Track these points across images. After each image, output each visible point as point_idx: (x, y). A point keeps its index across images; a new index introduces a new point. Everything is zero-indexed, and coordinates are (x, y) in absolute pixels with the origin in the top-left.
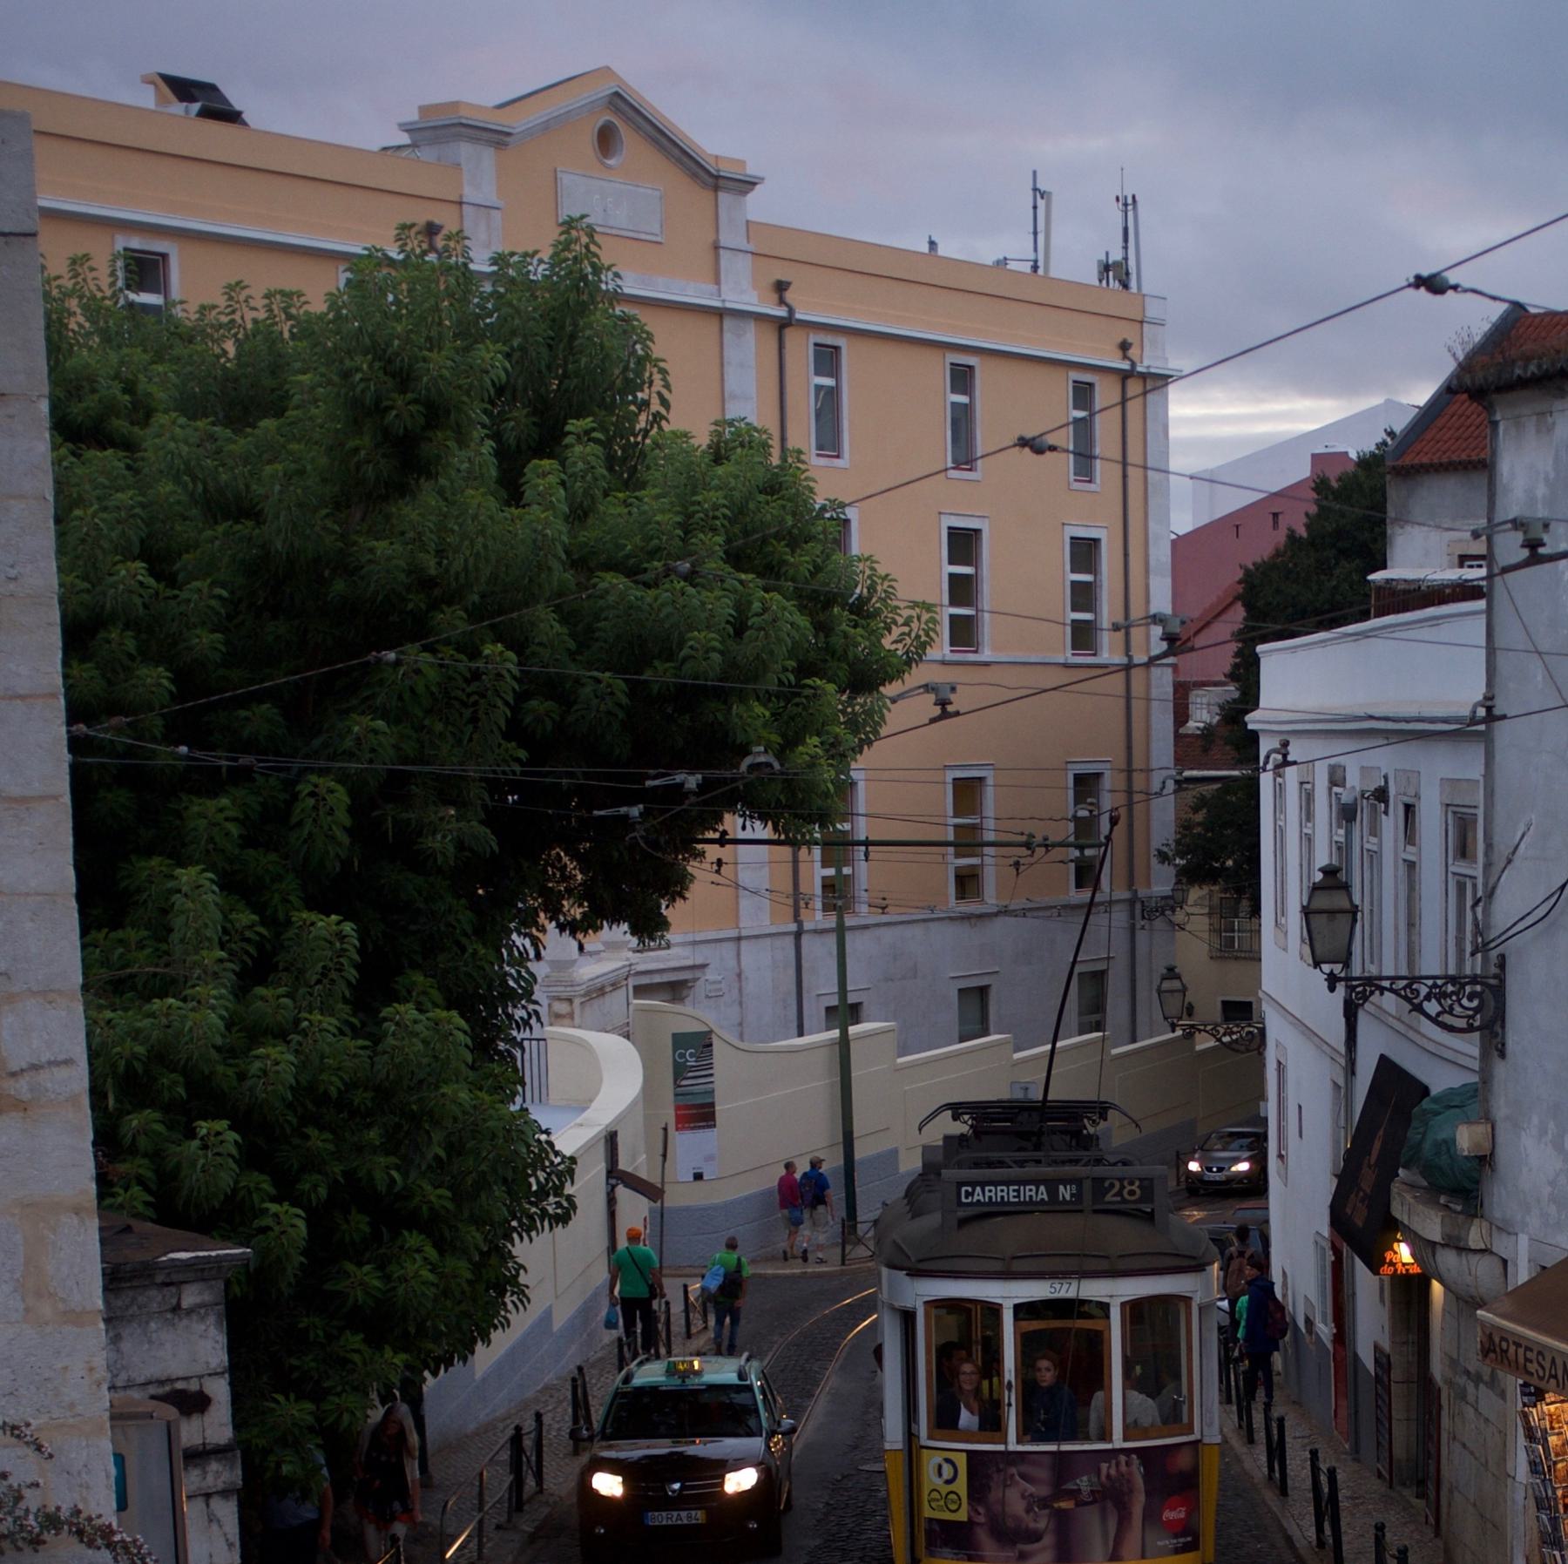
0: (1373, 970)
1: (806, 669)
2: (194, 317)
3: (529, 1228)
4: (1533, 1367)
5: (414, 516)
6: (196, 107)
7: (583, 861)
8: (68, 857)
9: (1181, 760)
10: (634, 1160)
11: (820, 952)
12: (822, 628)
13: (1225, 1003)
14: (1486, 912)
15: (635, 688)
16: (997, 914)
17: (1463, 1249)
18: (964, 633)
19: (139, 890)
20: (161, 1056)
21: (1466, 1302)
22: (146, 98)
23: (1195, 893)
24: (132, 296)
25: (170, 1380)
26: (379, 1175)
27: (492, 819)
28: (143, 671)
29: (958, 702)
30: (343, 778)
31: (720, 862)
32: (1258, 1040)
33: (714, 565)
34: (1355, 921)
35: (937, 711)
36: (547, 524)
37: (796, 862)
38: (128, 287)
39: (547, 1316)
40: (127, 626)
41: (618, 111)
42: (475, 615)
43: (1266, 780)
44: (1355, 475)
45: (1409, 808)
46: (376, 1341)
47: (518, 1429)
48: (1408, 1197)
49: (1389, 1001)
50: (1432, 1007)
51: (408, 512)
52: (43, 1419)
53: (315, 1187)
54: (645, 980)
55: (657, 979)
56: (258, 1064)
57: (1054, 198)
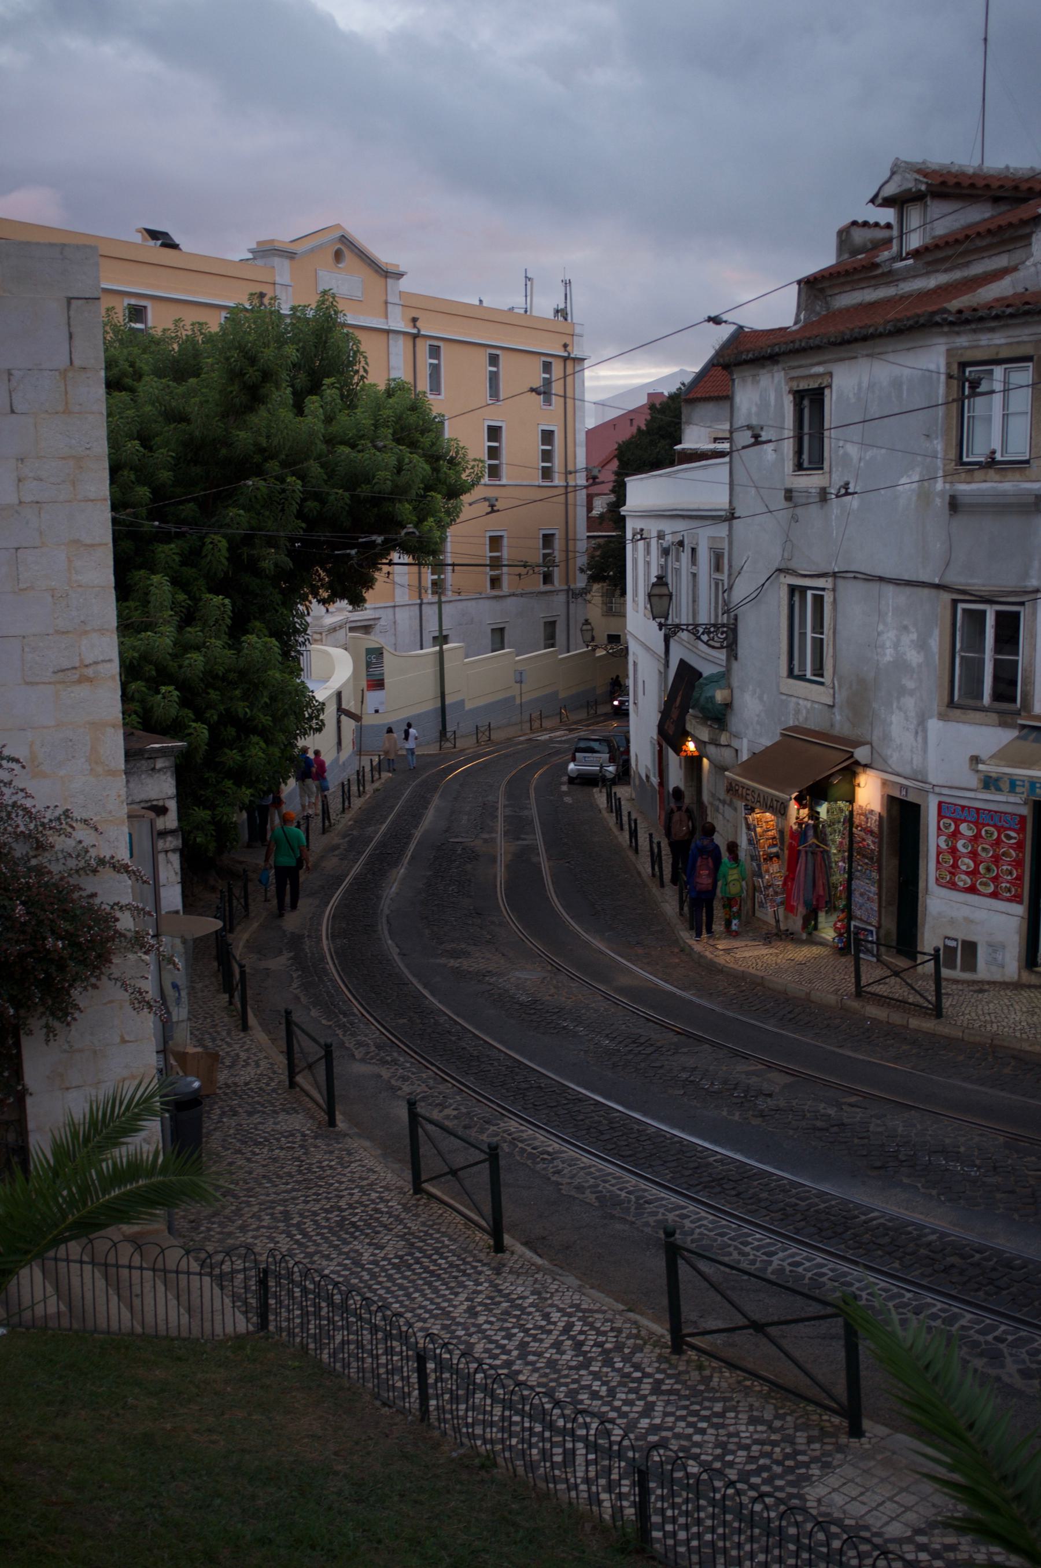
0: (677, 621)
1: (428, 488)
2: (160, 334)
4: (749, 798)
5: (256, 421)
6: (159, 242)
8: (111, 570)
10: (349, 704)
11: (430, 613)
12: (436, 470)
14: (729, 596)
17: (718, 745)
18: (494, 472)
19: (135, 584)
20: (145, 657)
21: (719, 768)
22: (138, 238)
23: (596, 587)
24: (133, 325)
25: (150, 801)
26: (240, 710)
27: (290, 553)
28: (138, 489)
29: (499, 506)
30: (225, 536)
31: (389, 573)
35: (489, 509)
37: (420, 573)
38: (130, 321)
40: (131, 469)
41: (343, 243)
42: (284, 464)
45: (693, 550)
46: (238, 784)
48: (694, 722)
49: (684, 635)
50: (705, 638)
51: (254, 419)
52: (99, 818)
54: (353, 625)
55: (359, 624)
56: (187, 662)
57: (535, 282)
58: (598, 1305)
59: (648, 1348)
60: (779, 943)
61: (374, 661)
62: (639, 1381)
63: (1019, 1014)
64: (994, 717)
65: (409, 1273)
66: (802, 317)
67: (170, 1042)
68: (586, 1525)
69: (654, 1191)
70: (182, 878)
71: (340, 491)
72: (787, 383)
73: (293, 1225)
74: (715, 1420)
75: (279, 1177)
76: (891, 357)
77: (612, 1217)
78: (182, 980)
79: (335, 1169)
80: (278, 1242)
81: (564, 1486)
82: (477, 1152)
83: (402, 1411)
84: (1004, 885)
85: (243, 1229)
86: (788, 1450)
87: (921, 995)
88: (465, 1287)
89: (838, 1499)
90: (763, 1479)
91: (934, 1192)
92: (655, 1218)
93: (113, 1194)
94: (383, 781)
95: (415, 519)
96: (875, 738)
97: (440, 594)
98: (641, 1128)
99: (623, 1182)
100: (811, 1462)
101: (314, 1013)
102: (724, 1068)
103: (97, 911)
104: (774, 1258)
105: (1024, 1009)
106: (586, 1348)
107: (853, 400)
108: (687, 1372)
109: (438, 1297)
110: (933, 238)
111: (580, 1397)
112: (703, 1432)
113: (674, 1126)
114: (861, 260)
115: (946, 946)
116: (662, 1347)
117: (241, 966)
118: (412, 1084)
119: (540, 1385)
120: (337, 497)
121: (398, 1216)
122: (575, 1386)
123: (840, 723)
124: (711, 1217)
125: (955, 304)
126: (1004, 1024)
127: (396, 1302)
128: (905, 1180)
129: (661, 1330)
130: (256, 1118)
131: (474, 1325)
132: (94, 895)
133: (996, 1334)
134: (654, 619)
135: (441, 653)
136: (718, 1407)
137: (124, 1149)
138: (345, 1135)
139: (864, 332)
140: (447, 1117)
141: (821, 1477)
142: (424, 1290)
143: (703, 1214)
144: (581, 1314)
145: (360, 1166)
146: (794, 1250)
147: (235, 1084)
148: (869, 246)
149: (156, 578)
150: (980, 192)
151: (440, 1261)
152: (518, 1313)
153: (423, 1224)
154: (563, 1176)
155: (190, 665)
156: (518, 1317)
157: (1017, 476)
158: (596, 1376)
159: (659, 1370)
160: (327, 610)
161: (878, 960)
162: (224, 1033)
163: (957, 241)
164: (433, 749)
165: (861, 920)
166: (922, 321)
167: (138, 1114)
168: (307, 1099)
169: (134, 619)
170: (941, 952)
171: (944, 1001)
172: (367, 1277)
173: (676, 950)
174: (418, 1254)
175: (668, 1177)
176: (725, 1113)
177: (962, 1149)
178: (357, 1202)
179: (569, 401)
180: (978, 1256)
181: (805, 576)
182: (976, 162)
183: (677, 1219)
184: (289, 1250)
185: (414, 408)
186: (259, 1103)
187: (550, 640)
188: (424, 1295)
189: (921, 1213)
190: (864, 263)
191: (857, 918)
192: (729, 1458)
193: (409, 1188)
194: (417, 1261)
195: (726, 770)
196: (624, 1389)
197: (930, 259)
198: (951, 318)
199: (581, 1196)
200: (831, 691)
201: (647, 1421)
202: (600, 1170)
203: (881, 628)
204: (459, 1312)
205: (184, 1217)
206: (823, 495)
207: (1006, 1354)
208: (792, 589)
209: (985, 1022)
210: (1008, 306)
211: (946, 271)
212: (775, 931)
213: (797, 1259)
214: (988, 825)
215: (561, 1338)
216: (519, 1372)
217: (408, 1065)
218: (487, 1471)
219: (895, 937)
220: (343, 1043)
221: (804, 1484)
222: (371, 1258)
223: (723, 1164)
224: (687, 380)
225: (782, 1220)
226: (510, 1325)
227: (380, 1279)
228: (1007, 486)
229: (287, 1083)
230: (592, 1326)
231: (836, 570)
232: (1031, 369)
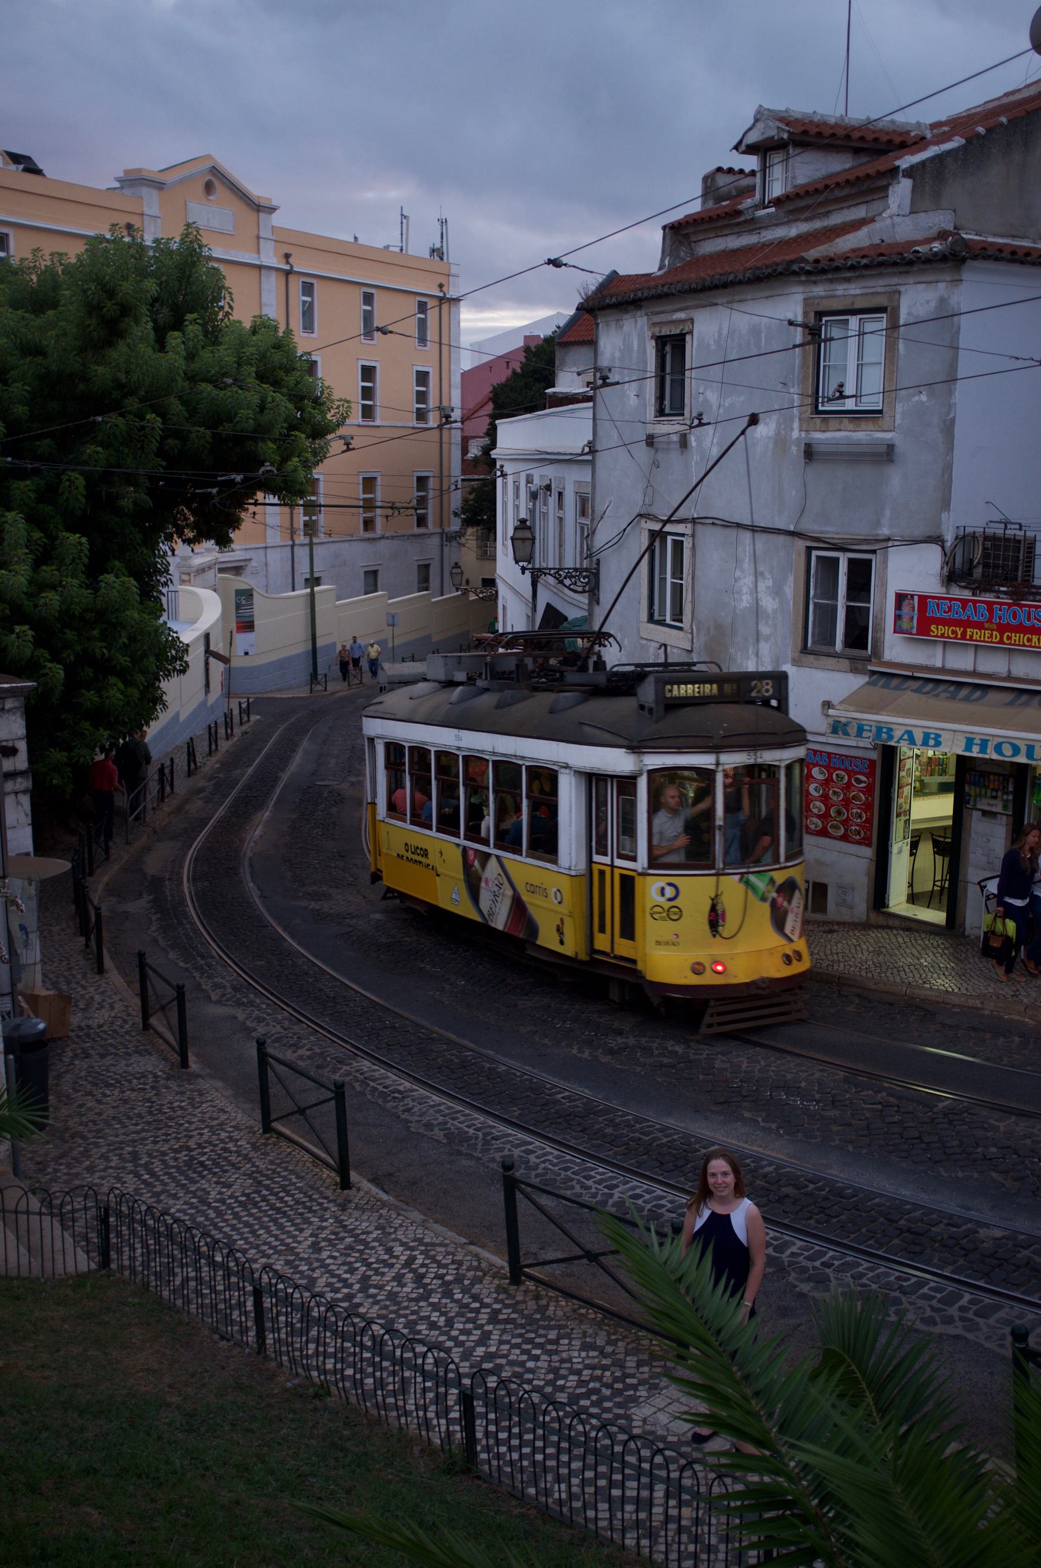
0: (544, 565)
1: (292, 427)
3: (168, 675)
5: (115, 356)
6: (21, 167)
7: (194, 512)
9: (464, 471)
11: (302, 554)
13: (483, 580)
14: (592, 540)
15: (214, 436)
16: (380, 538)
18: (368, 412)
23: (470, 530)
26: (97, 650)
29: (354, 444)
30: (82, 473)
31: (254, 513)
32: (495, 597)
33: (252, 381)
34: (534, 543)
35: (345, 447)
36: (176, 361)
37: (292, 514)
39: (178, 714)
41: (214, 175)
43: (499, 481)
44: (542, 346)
45: (560, 494)
47: (162, 765)
49: (551, 580)
50: (567, 582)
53: (68, 656)
54: (224, 566)
55: (229, 565)
56: (43, 600)
58: (441, 1238)
59: (487, 1280)
61: (244, 602)
62: (477, 1311)
63: (866, 953)
64: (845, 663)
65: (255, 1211)
66: (667, 262)
71: (202, 429)
72: (649, 329)
73: (141, 1165)
74: (549, 1347)
75: (130, 1118)
76: (742, 307)
77: (460, 1153)
78: (32, 923)
79: (186, 1110)
80: (125, 1182)
83: (240, 1344)
84: (853, 828)
85: (91, 1169)
86: (618, 1374)
88: (310, 1223)
89: (663, 1418)
90: (592, 1401)
91: (774, 1126)
92: (501, 1154)
94: (251, 723)
95: (278, 458)
97: (311, 536)
99: (472, 1119)
100: (639, 1384)
101: (172, 955)
104: (615, 1191)
105: (871, 949)
106: (426, 1281)
107: (713, 347)
108: (525, 1302)
109: (282, 1234)
110: (795, 187)
111: (419, 1328)
112: (536, 1358)
114: (724, 207)
118: (268, 1025)
119: (379, 1317)
120: (198, 435)
121: (247, 1155)
122: (414, 1317)
124: (556, 1153)
125: (813, 254)
127: (241, 1239)
129: (501, 1262)
130: (109, 1061)
131: (317, 1260)
133: (823, 1260)
134: (517, 562)
135: (312, 595)
136: (552, 1335)
138: (198, 1076)
139: (724, 279)
140: (301, 1058)
141: (648, 1398)
143: (549, 1149)
144: (423, 1248)
145: (211, 1106)
146: (635, 1183)
147: (89, 1027)
149: (10, 516)
151: (286, 1199)
152: (362, 1247)
153: (272, 1162)
154: (413, 1114)
156: (361, 1252)
157: (871, 426)
158: (435, 1307)
160: (193, 551)
162: (79, 976)
163: (816, 191)
164: (304, 693)
166: (780, 269)
168: (161, 1041)
172: (213, 1215)
174: (265, 1192)
175: (516, 1114)
176: (575, 1051)
177: (803, 1084)
178: (206, 1142)
180: (811, 1186)
182: (840, 111)
183: (523, 1154)
185: (278, 346)
186: (111, 1045)
187: (424, 583)
192: (560, 1382)
193: (258, 1128)
194: (264, 1199)
196: (461, 1319)
197: (791, 208)
199: (429, 1133)
200: (690, 636)
201: (483, 1349)
202: (450, 1108)
203: (738, 573)
204: (303, 1248)
205: (31, 1159)
207: (832, 1279)
208: (653, 535)
209: (833, 961)
210: (863, 257)
211: (806, 220)
213: (638, 1191)
216: (360, 1305)
217: (264, 1006)
218: (320, 1400)
220: (200, 985)
222: (218, 1196)
224: (562, 323)
226: (353, 1260)
227: (226, 1217)
229: (141, 1025)
230: (434, 1259)
231: (696, 516)
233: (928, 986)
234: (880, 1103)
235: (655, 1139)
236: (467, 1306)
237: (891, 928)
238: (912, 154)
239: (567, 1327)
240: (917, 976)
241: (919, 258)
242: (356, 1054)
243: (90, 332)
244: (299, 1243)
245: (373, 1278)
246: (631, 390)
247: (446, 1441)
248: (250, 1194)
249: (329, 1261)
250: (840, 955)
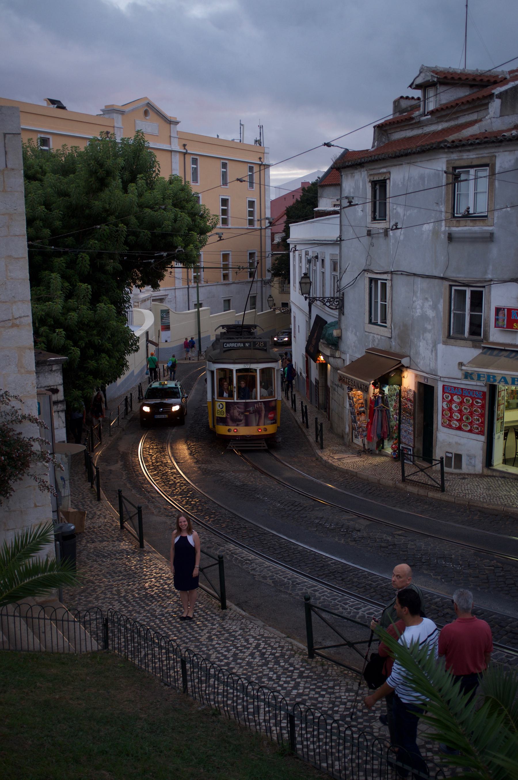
0: (315, 296)
1: (190, 230)
3: (129, 352)
4: (350, 383)
5: (104, 196)
6: (56, 106)
7: (141, 272)
9: (273, 250)
10: (152, 338)
11: (193, 292)
12: (194, 220)
13: (282, 303)
14: (340, 283)
15: (153, 234)
17: (334, 357)
18: (225, 221)
20: (48, 315)
21: (335, 369)
22: (45, 104)
23: (276, 279)
24: (42, 147)
25: (50, 386)
28: (44, 230)
29: (223, 237)
30: (88, 254)
31: (171, 272)
35: (219, 239)
36: (133, 198)
37: (188, 272)
39: (133, 372)
41: (148, 107)
42: (117, 218)
43: (291, 254)
45: (323, 260)
46: (95, 378)
47: (127, 397)
48: (323, 346)
49: (318, 303)
50: (328, 304)
52: (22, 395)
53: (82, 343)
54: (155, 298)
55: (157, 298)
56: (69, 317)
58: (272, 634)
59: (297, 656)
60: (365, 456)
61: (165, 316)
62: (292, 672)
64: (470, 343)
66: (376, 144)
67: (61, 507)
68: (264, 742)
69: (301, 578)
70: (66, 425)
72: (368, 177)
73: (122, 597)
74: (329, 690)
76: (419, 164)
78: (67, 476)
81: (254, 724)
82: (214, 560)
83: (174, 688)
84: (475, 426)
85: (97, 599)
87: (435, 481)
88: (207, 626)
91: (439, 577)
92: (301, 592)
93: (26, 582)
95: (183, 245)
96: (412, 353)
97: (198, 283)
98: (295, 547)
100: (376, 710)
102: (337, 517)
103: (21, 442)
104: (360, 611)
105: (485, 487)
106: (266, 656)
107: (401, 186)
108: (316, 667)
109: (193, 632)
111: (263, 680)
112: (323, 696)
113: (311, 546)
114: (405, 116)
115: (446, 457)
116: (304, 655)
117: (97, 469)
119: (243, 674)
120: (145, 234)
122: (261, 674)
123: (395, 346)
124: (329, 591)
125: (451, 138)
126: (475, 494)
128: (425, 572)
129: (304, 647)
130: (105, 544)
131: (211, 645)
132: (20, 433)
136: (331, 684)
137: (31, 560)
142: (186, 628)
143: (325, 589)
144: (264, 639)
146: (370, 607)
148: (409, 109)
149: (53, 275)
150: (457, 82)
152: (233, 639)
154: (256, 571)
155: (71, 318)
156: (233, 641)
157: (481, 223)
158: (271, 669)
159: (302, 666)
161: (413, 464)
163: (452, 106)
165: (405, 443)
166: (434, 146)
167: (39, 542)
169: (42, 296)
170: (444, 459)
171: (445, 483)
173: (314, 459)
176: (337, 540)
177: (453, 556)
179: (262, 186)
181: (377, 273)
182: (462, 67)
183: (312, 592)
184: (119, 609)
185: (183, 189)
186: (106, 537)
188: (186, 631)
189: (433, 588)
190: (406, 117)
191: (403, 443)
192: (336, 709)
195: (339, 369)
198: (448, 145)
199: (265, 581)
200: (390, 330)
201: (296, 691)
202: (275, 568)
203: (415, 299)
205: (67, 593)
206: (386, 232)
208: (371, 280)
209: (466, 494)
210: (477, 139)
211: (446, 121)
212: (362, 449)
213: (371, 611)
214: (467, 396)
215: (254, 651)
216: (233, 668)
219: (421, 451)
221: (372, 721)
223: (335, 565)
225: (364, 592)
226: (229, 645)
227: (165, 623)
228: (476, 229)
230: (270, 645)
231: (393, 270)
232: (488, 170)
233: (515, 506)
234: (493, 566)
235: (378, 584)
236: (287, 669)
237: (495, 477)
238: (501, 86)
239: (338, 680)
240: (509, 501)
241: (506, 139)
242: (227, 541)
243: (91, 185)
244: (202, 636)
245: (239, 654)
246: (359, 208)
247: (280, 738)
248: (176, 611)
249: (217, 646)
250: (469, 491)
